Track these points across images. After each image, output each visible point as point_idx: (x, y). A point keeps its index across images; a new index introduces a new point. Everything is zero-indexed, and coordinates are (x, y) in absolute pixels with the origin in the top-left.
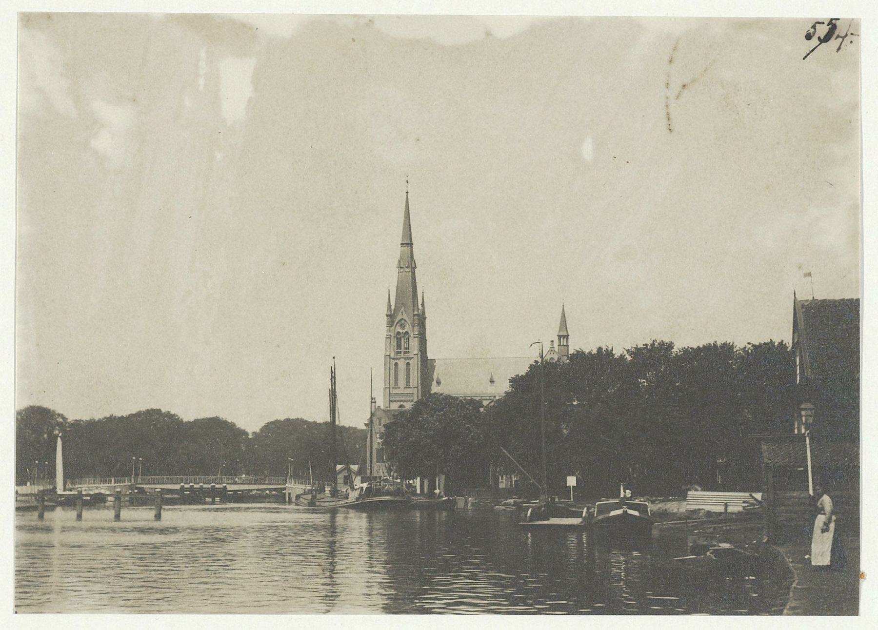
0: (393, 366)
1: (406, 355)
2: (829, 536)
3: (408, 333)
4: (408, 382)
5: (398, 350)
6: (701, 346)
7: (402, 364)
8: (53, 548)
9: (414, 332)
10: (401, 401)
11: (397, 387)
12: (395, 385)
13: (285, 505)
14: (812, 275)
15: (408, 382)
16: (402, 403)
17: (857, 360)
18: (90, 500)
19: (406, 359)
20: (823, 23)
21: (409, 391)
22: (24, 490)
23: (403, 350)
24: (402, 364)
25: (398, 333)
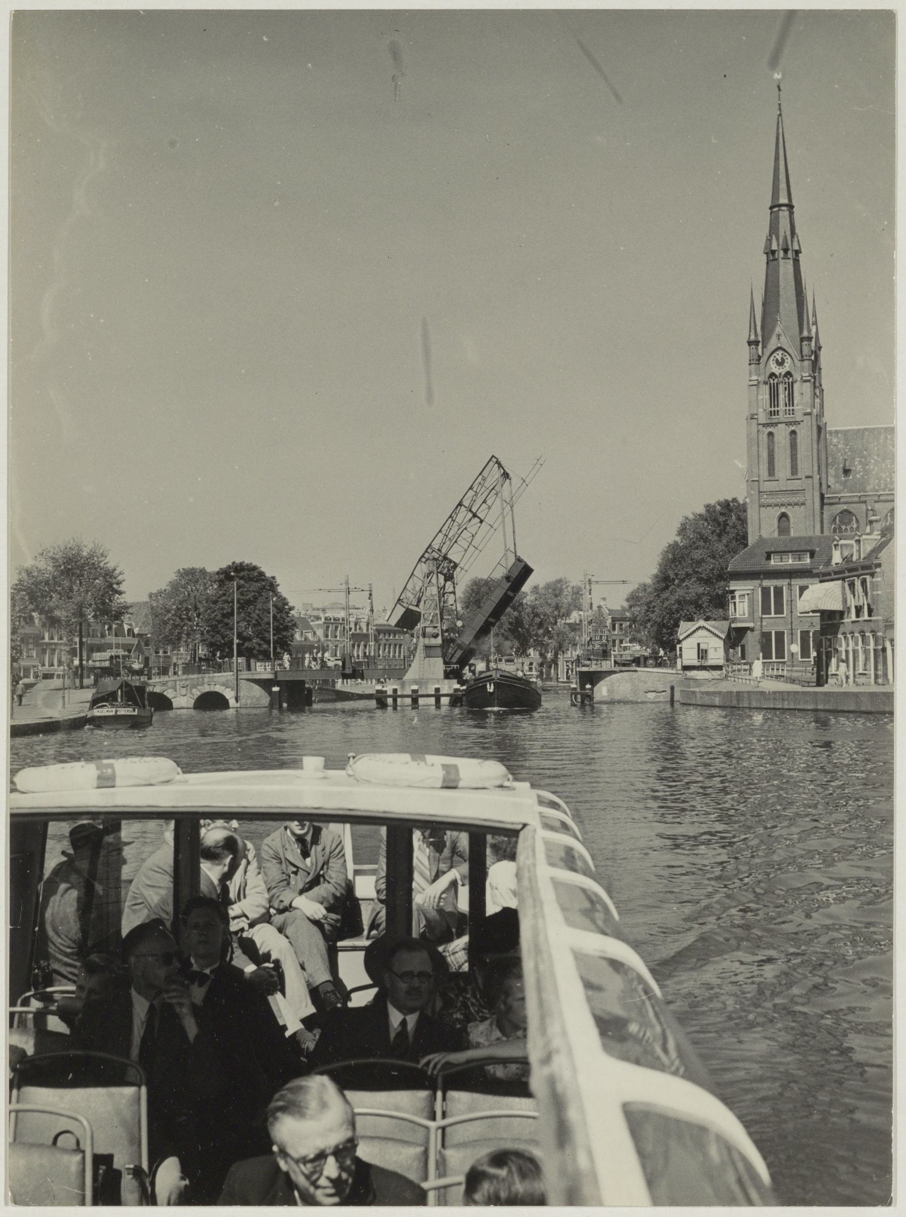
0: (764, 438)
1: (789, 417)
2: (467, 888)
3: (791, 376)
4: (794, 469)
5: (772, 409)
6: (691, 517)
7: (782, 434)
8: (662, 925)
9: (801, 371)
10: (783, 505)
11: (795, 477)
12: (792, 474)
13: (869, 650)
14: (511, 475)
15: (794, 469)
16: (783, 510)
17: (32, 759)
18: (225, 961)
19: (788, 424)
20: (779, 100)
21: (796, 485)
22: (823, 623)
23: (782, 407)
24: (782, 434)
25: (772, 375)
